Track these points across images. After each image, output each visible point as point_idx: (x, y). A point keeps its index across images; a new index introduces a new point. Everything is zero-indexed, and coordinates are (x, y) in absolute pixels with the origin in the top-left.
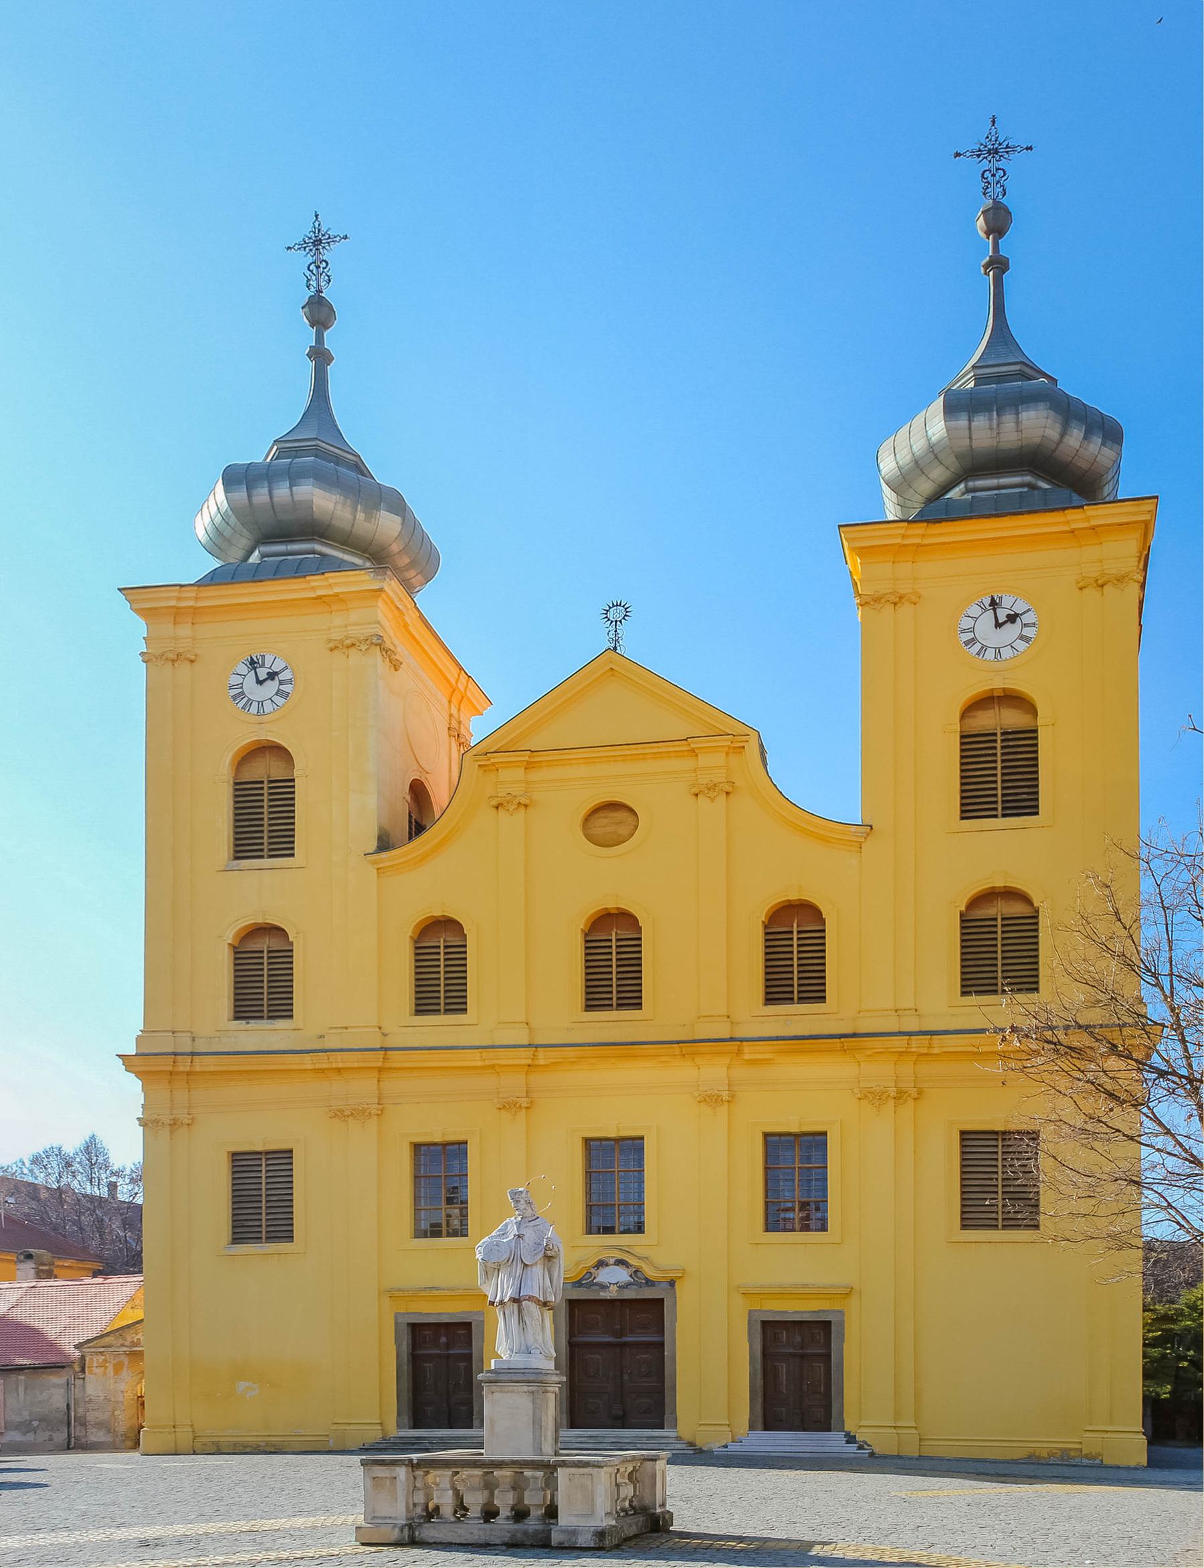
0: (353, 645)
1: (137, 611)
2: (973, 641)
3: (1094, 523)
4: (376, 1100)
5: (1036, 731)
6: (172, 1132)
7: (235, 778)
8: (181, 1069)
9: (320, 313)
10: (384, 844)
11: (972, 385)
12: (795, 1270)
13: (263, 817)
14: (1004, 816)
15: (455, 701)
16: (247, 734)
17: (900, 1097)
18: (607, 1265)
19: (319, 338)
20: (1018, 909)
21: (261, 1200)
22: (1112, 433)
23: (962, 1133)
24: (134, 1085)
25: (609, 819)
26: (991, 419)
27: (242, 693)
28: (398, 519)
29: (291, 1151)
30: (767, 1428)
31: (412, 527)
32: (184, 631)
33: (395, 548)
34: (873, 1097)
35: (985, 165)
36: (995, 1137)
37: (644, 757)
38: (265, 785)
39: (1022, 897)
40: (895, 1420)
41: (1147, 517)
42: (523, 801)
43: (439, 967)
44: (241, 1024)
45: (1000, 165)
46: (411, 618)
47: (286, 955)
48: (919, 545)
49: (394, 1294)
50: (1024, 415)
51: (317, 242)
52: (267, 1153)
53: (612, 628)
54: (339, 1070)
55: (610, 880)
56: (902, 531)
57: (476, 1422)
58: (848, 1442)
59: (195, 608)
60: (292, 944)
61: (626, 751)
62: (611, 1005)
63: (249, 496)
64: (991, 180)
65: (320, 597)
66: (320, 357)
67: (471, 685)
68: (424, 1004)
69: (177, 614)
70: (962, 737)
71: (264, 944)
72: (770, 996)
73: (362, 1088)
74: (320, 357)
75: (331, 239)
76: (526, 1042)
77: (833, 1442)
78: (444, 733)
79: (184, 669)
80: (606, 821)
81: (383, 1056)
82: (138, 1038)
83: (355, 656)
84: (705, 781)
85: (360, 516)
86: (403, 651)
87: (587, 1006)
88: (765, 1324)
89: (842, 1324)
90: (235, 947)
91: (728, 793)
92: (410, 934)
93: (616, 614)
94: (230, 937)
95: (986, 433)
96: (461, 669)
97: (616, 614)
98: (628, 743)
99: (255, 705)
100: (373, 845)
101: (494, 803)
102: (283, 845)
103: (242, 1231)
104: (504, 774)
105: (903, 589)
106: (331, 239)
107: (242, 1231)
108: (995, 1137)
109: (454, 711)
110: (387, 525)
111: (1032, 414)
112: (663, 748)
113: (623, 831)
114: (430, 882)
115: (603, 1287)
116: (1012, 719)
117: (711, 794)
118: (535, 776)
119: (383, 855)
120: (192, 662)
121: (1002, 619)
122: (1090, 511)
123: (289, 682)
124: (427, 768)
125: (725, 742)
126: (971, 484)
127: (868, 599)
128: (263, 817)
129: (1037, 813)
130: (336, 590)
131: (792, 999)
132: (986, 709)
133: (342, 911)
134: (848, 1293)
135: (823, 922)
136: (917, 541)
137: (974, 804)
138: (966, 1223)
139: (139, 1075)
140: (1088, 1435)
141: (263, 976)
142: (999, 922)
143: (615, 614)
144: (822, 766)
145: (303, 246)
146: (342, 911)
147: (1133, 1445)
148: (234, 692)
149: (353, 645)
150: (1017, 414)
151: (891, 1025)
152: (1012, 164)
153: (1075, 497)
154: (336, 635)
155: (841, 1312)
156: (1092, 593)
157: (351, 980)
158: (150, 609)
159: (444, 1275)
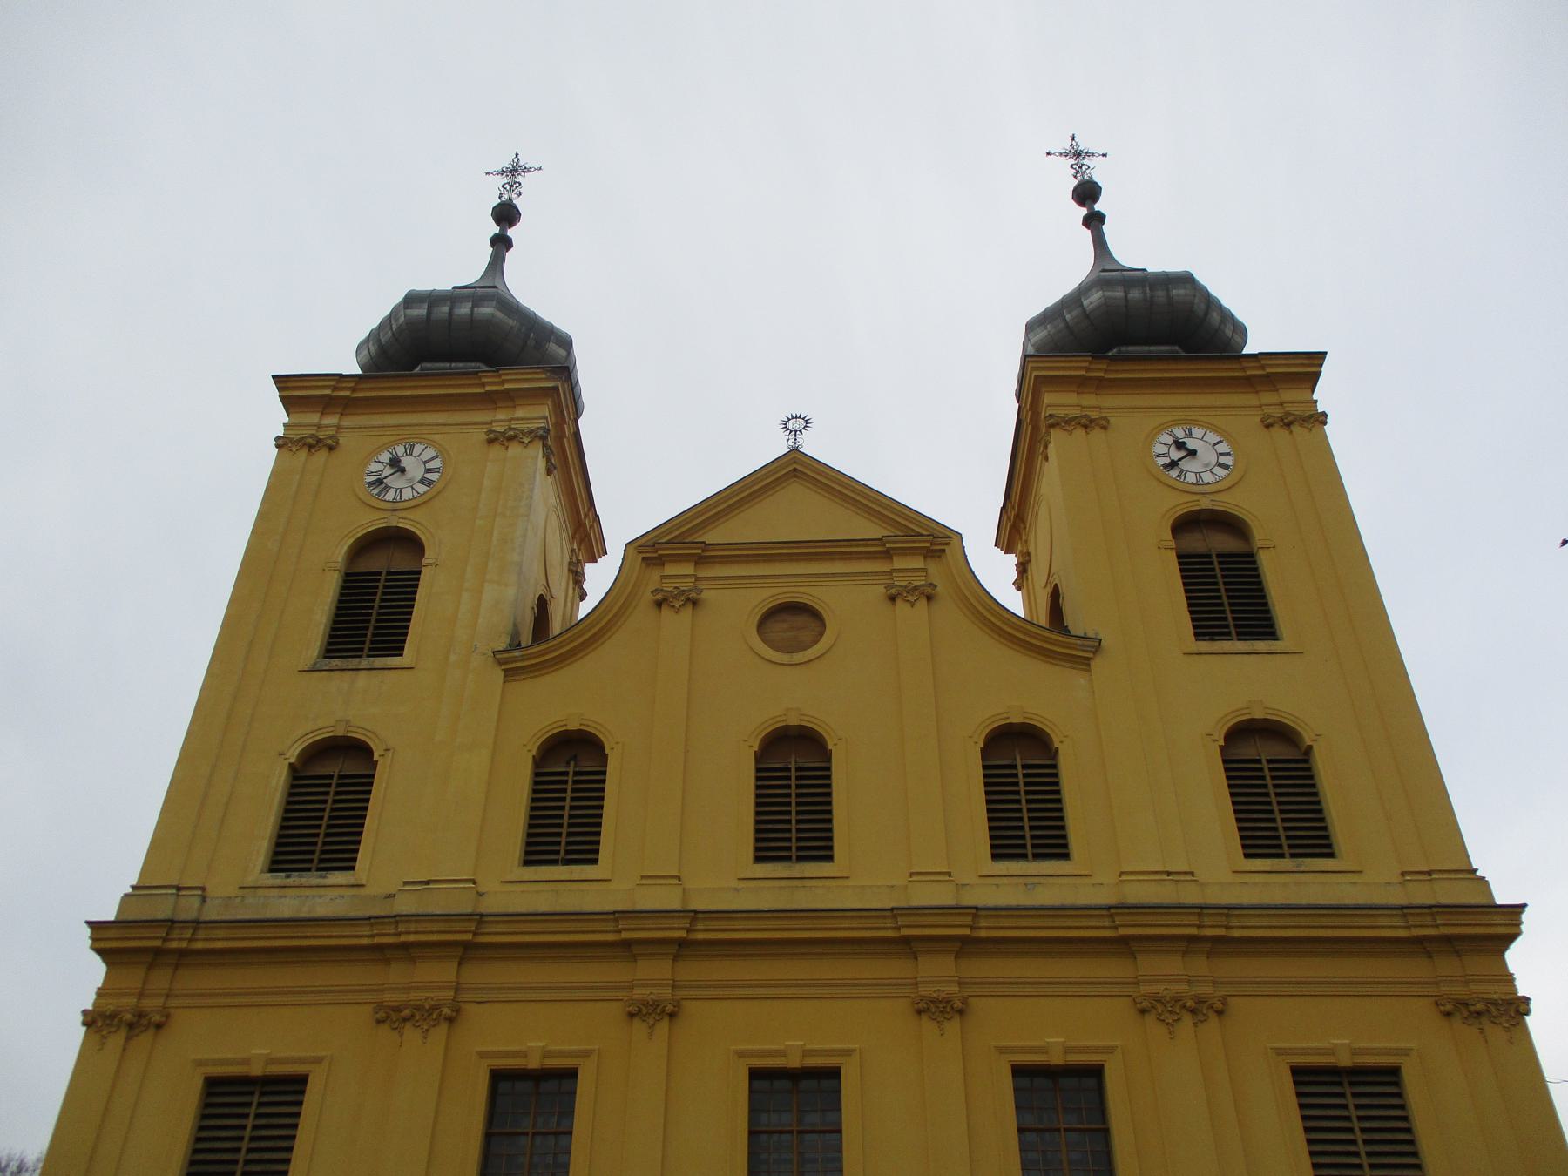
9: (506, 214)
20: (1280, 751)
32: (331, 420)
34: (1157, 1008)
38: (383, 577)
42: (693, 595)
47: (365, 782)
48: (1100, 379)
53: (792, 437)
54: (405, 946)
69: (326, 404)
71: (334, 768)
73: (434, 978)
75: (526, 170)
76: (469, 911)
79: (321, 456)
81: (473, 941)
83: (515, 450)
92: (756, 748)
94: (293, 755)
102: (391, 640)
104: (670, 569)
106: (526, 170)
108: (1336, 1079)
121: (1183, 453)
123: (1228, 454)
128: (373, 606)
131: (1229, 633)
137: (1207, 625)
141: (326, 801)
143: (798, 424)
145: (501, 173)
154: (499, 428)
156: (1279, 433)
157: (441, 830)
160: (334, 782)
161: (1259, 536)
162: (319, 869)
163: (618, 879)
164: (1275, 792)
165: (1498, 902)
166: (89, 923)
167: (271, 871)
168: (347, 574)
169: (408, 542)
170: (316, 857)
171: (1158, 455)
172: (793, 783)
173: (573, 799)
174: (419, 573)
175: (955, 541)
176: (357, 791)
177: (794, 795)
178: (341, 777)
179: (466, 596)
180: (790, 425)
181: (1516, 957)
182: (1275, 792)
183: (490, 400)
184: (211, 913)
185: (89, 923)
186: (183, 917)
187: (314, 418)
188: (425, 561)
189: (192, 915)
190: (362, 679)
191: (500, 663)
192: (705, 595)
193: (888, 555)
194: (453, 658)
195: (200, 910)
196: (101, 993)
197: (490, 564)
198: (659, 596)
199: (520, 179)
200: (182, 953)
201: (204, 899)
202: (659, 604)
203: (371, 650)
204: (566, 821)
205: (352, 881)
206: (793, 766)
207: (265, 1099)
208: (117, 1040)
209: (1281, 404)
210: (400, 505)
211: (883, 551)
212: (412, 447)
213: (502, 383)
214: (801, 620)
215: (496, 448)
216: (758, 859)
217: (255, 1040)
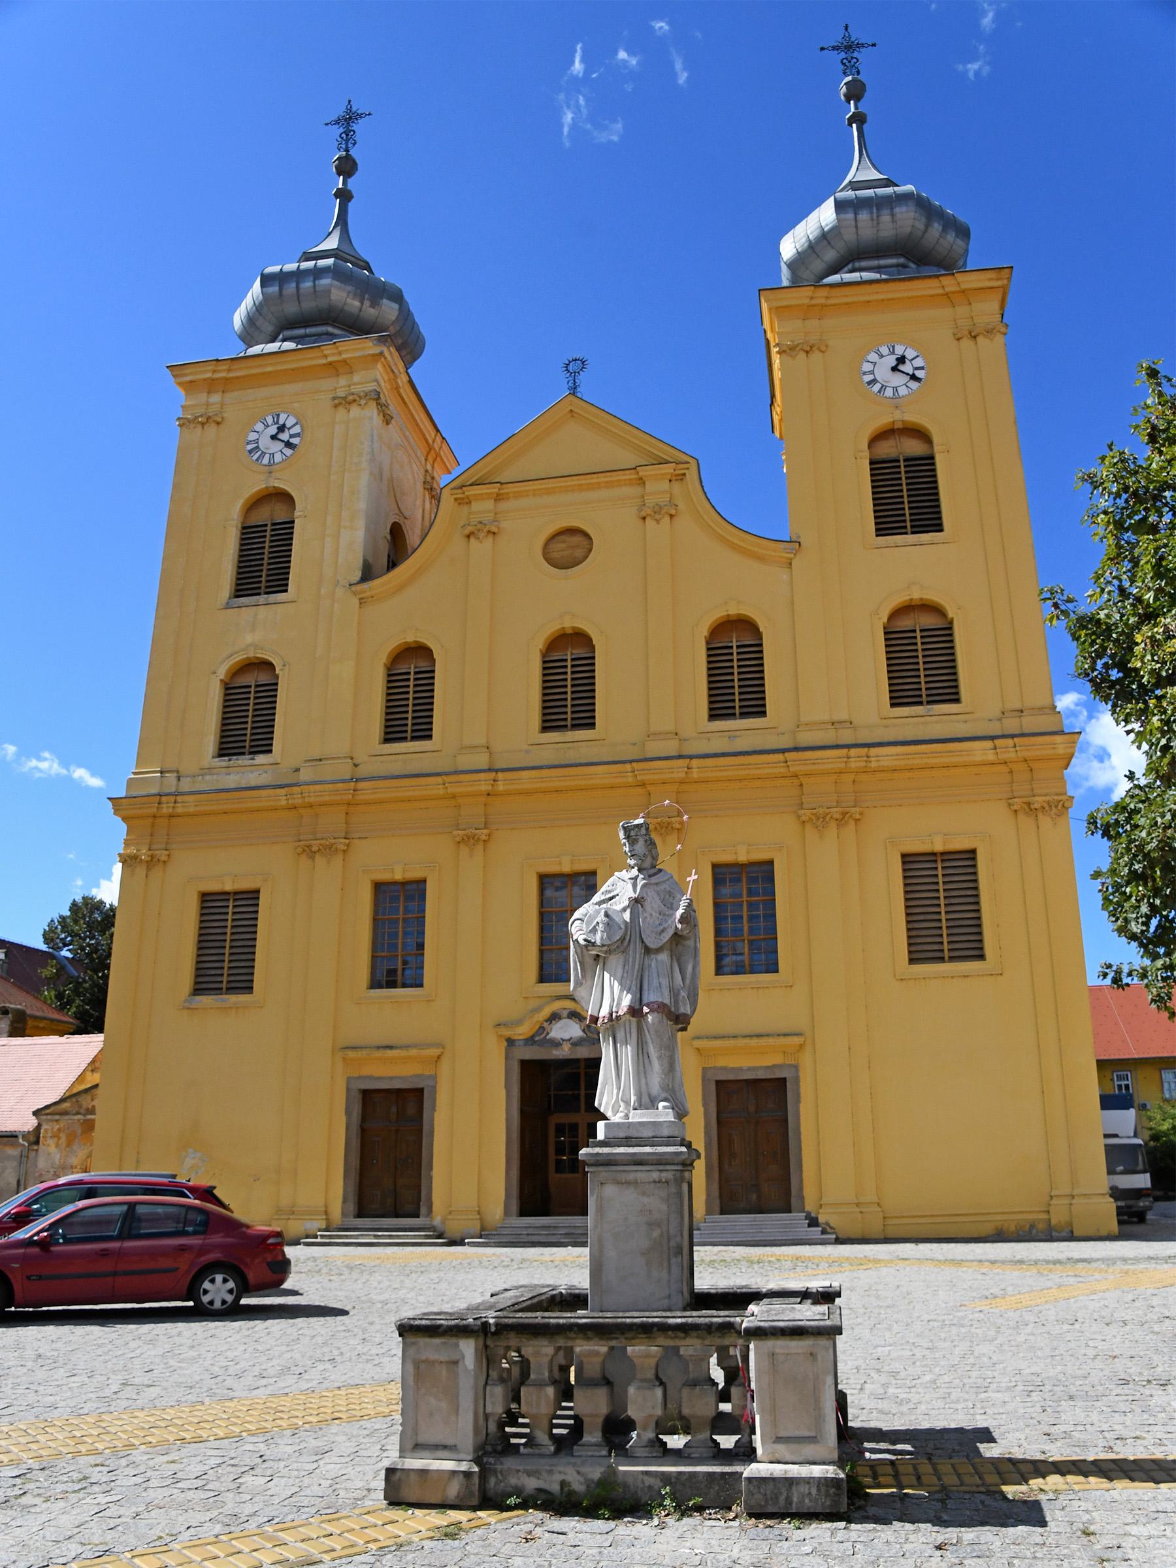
1: (180, 384)
2: (874, 381)
3: (963, 286)
5: (932, 458)
6: (148, 869)
7: (243, 523)
8: (165, 811)
10: (368, 574)
13: (264, 560)
14: (913, 533)
15: (430, 459)
16: (256, 484)
17: (841, 822)
18: (560, 1018)
20: (928, 621)
21: (226, 946)
22: (964, 232)
23: (903, 856)
24: (120, 829)
25: (568, 547)
26: (872, 213)
27: (257, 447)
28: (396, 306)
31: (405, 315)
32: (215, 398)
35: (843, 55)
36: (933, 858)
37: (598, 486)
39: (935, 609)
42: (494, 529)
43: (408, 703)
44: (223, 762)
45: (855, 54)
46: (403, 380)
47: (272, 688)
50: (897, 210)
51: (348, 120)
52: (236, 893)
55: (565, 601)
56: (810, 294)
57: (423, 1210)
58: (810, 1225)
59: (227, 379)
61: (583, 481)
62: (566, 726)
63: (281, 290)
65: (330, 364)
67: (445, 446)
68: (392, 733)
69: (211, 386)
70: (871, 463)
71: (249, 679)
72: (714, 712)
75: (360, 116)
77: (797, 1219)
78: (420, 487)
79: (212, 429)
80: (563, 545)
83: (355, 411)
85: (367, 303)
86: (394, 408)
88: (719, 1083)
89: (797, 1080)
90: (226, 684)
91: (671, 516)
94: (222, 672)
95: (867, 227)
96: (438, 431)
99: (267, 456)
100: (358, 574)
102: (279, 583)
106: (360, 116)
108: (933, 858)
109: (429, 467)
110: (389, 310)
111: (904, 209)
112: (615, 477)
113: (579, 553)
114: (408, 609)
115: (556, 1044)
116: (914, 447)
118: (503, 506)
119: (365, 586)
123: (922, 368)
124: (406, 514)
125: (668, 469)
127: (785, 348)
128: (264, 560)
129: (941, 530)
130: (344, 356)
132: (886, 439)
136: (823, 301)
137: (888, 522)
141: (248, 713)
142: (918, 634)
145: (336, 123)
147: (1114, 1226)
148: (249, 447)
149: (355, 401)
150: (892, 209)
151: (829, 737)
152: (862, 55)
155: (796, 1067)
157: (328, 715)
158: (191, 382)
162: (251, 753)
167: (220, 755)
168: (244, 528)
169: (285, 498)
171: (865, 373)
172: (569, 670)
173: (415, 692)
174: (293, 522)
177: (568, 686)
178: (257, 686)
179: (328, 539)
180: (570, 368)
183: (334, 368)
184: (185, 785)
186: (167, 791)
187: (202, 397)
188: (297, 514)
189: (173, 790)
190: (262, 612)
191: (355, 593)
192: (503, 524)
194: (323, 591)
195: (178, 786)
196: (127, 843)
197: (343, 513)
198: (467, 532)
199: (355, 127)
201: (179, 778)
203: (228, 989)
204: (410, 709)
205: (272, 761)
206: (569, 658)
207: (237, 903)
208: (141, 871)
209: (857, 1205)
212: (278, 416)
214: (576, 539)
215: (341, 410)
217: (227, 871)
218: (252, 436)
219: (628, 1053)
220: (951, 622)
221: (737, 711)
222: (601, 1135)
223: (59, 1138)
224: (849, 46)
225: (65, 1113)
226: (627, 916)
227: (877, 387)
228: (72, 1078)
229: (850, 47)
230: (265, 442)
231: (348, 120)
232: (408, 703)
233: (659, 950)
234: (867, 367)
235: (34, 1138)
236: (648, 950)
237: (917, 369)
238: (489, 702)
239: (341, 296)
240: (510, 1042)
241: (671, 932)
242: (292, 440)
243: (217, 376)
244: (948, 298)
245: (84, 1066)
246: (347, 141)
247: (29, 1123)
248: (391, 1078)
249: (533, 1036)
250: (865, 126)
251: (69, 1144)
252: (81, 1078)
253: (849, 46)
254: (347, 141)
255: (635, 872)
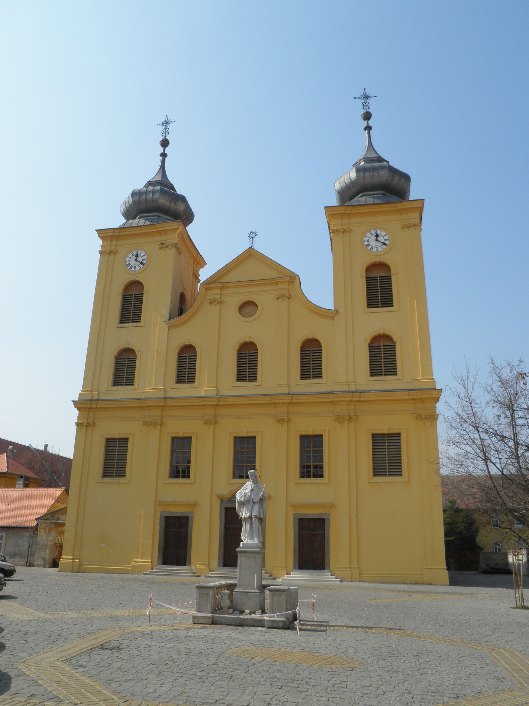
0: (167, 247)
1: (100, 237)
2: (368, 245)
4: (160, 418)
7: (124, 293)
8: (93, 406)
9: (165, 143)
11: (363, 163)
12: (311, 495)
15: (195, 263)
17: (350, 419)
19: (164, 150)
21: (115, 459)
24: (76, 412)
27: (130, 264)
28: (184, 204)
29: (400, 434)
30: (165, 563)
33: (182, 214)
34: (339, 419)
40: (350, 565)
41: (421, 205)
42: (219, 300)
43: (186, 365)
45: (368, 101)
49: (161, 504)
51: (166, 123)
54: (148, 406)
60: (136, 356)
64: (365, 105)
65: (158, 231)
66: (164, 155)
70: (366, 278)
73: (156, 414)
74: (164, 155)
75: (170, 122)
78: (191, 274)
79: (112, 256)
82: (80, 394)
84: (281, 293)
85: (172, 204)
87: (238, 380)
89: (329, 519)
91: (288, 298)
93: (253, 235)
97: (253, 235)
98: (255, 279)
101: (209, 301)
102: (121, 473)
103: (106, 474)
105: (345, 227)
106: (170, 122)
107: (106, 474)
110: (181, 207)
114: (185, 334)
117: (283, 298)
118: (224, 292)
119: (171, 322)
120: (115, 253)
122: (404, 203)
123: (387, 240)
126: (365, 193)
128: (130, 305)
129: (392, 306)
133: (154, 340)
134: (332, 506)
135: (321, 346)
137: (372, 303)
138: (376, 474)
139: (78, 409)
140: (425, 570)
144: (319, 287)
145: (162, 124)
146: (154, 340)
148: (127, 263)
149: (167, 247)
152: (371, 101)
153: (398, 198)
155: (329, 514)
159: (178, 495)
160: (133, 296)
161: (393, 271)
163: (203, 386)
164: (382, 356)
165: (437, 388)
166: (73, 401)
170: (131, 319)
171: (365, 241)
175: (297, 278)
176: (133, 361)
177: (247, 361)
178: (383, 346)
181: (438, 405)
182: (382, 356)
185: (73, 401)
191: (167, 324)
193: (277, 283)
196: (78, 418)
199: (169, 127)
200: (95, 408)
202: (210, 303)
208: (84, 429)
210: (136, 272)
211: (274, 282)
213: (162, 227)
216: (371, 375)
217: (117, 431)
218: (128, 259)
219: (248, 526)
220: (395, 343)
221: (311, 376)
222: (241, 546)
223: (46, 529)
224: (365, 97)
225: (47, 519)
226: (249, 494)
227: (370, 247)
228: (50, 505)
229: (366, 97)
230: (133, 263)
231: (166, 123)
232: (186, 365)
233: (256, 503)
234: (366, 239)
235: (35, 529)
236: (254, 502)
237: (386, 240)
238: (215, 375)
239: (163, 201)
240: (222, 501)
241: (259, 498)
242: (143, 262)
243: (115, 234)
244: (399, 211)
245: (54, 501)
246: (166, 132)
247: (34, 523)
248: (177, 512)
249: (231, 499)
250: (371, 131)
251: (49, 532)
252: (53, 506)
253: (365, 97)
254: (166, 132)
255: (252, 483)
